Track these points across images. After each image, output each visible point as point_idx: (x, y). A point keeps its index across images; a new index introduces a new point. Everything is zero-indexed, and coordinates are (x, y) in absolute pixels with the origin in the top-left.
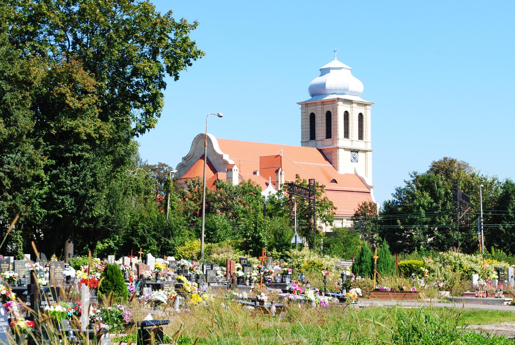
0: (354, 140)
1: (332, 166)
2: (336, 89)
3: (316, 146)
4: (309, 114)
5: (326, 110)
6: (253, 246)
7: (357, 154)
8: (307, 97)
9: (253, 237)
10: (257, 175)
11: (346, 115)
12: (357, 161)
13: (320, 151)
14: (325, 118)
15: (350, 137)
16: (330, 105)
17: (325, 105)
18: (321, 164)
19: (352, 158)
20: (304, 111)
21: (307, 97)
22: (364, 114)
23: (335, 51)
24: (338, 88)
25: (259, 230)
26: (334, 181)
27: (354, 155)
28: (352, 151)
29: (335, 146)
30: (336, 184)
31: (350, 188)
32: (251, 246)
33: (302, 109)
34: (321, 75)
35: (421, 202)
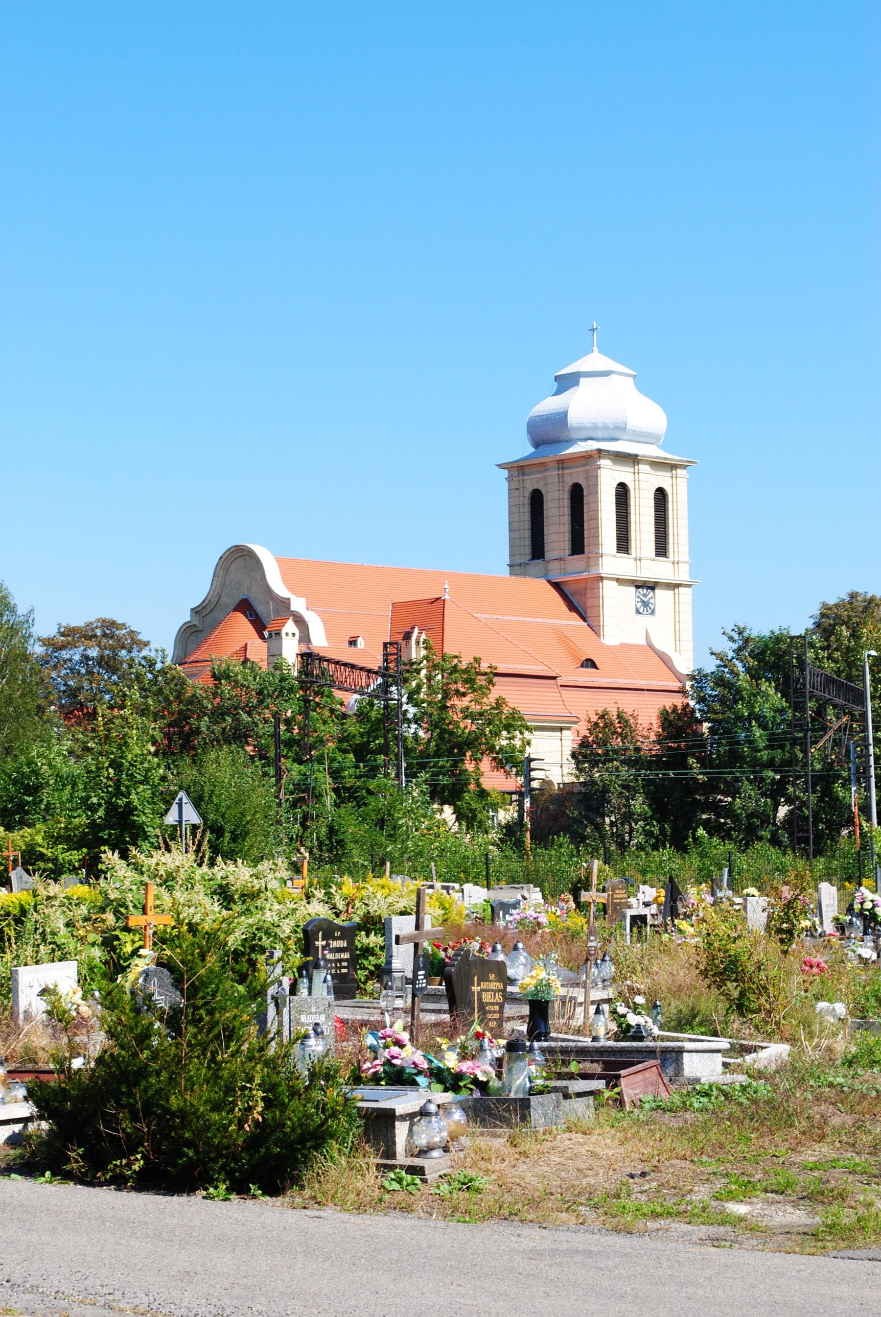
0: (642, 556)
1: (585, 624)
2: (595, 428)
3: (545, 575)
4: (527, 494)
5: (569, 482)
6: (110, 835)
7: (651, 595)
8: (523, 449)
9: (111, 808)
10: (359, 646)
11: (622, 492)
12: (653, 612)
13: (557, 586)
14: (567, 503)
15: (633, 550)
16: (579, 469)
17: (569, 468)
18: (557, 622)
19: (639, 605)
20: (515, 485)
21: (523, 449)
22: (669, 491)
23: (593, 330)
24: (600, 425)
25: (127, 787)
26: (590, 663)
27: (645, 595)
28: (637, 587)
29: (593, 572)
30: (594, 670)
31: (631, 681)
32: (105, 835)
33: (509, 479)
34: (558, 392)
35: (754, 707)
